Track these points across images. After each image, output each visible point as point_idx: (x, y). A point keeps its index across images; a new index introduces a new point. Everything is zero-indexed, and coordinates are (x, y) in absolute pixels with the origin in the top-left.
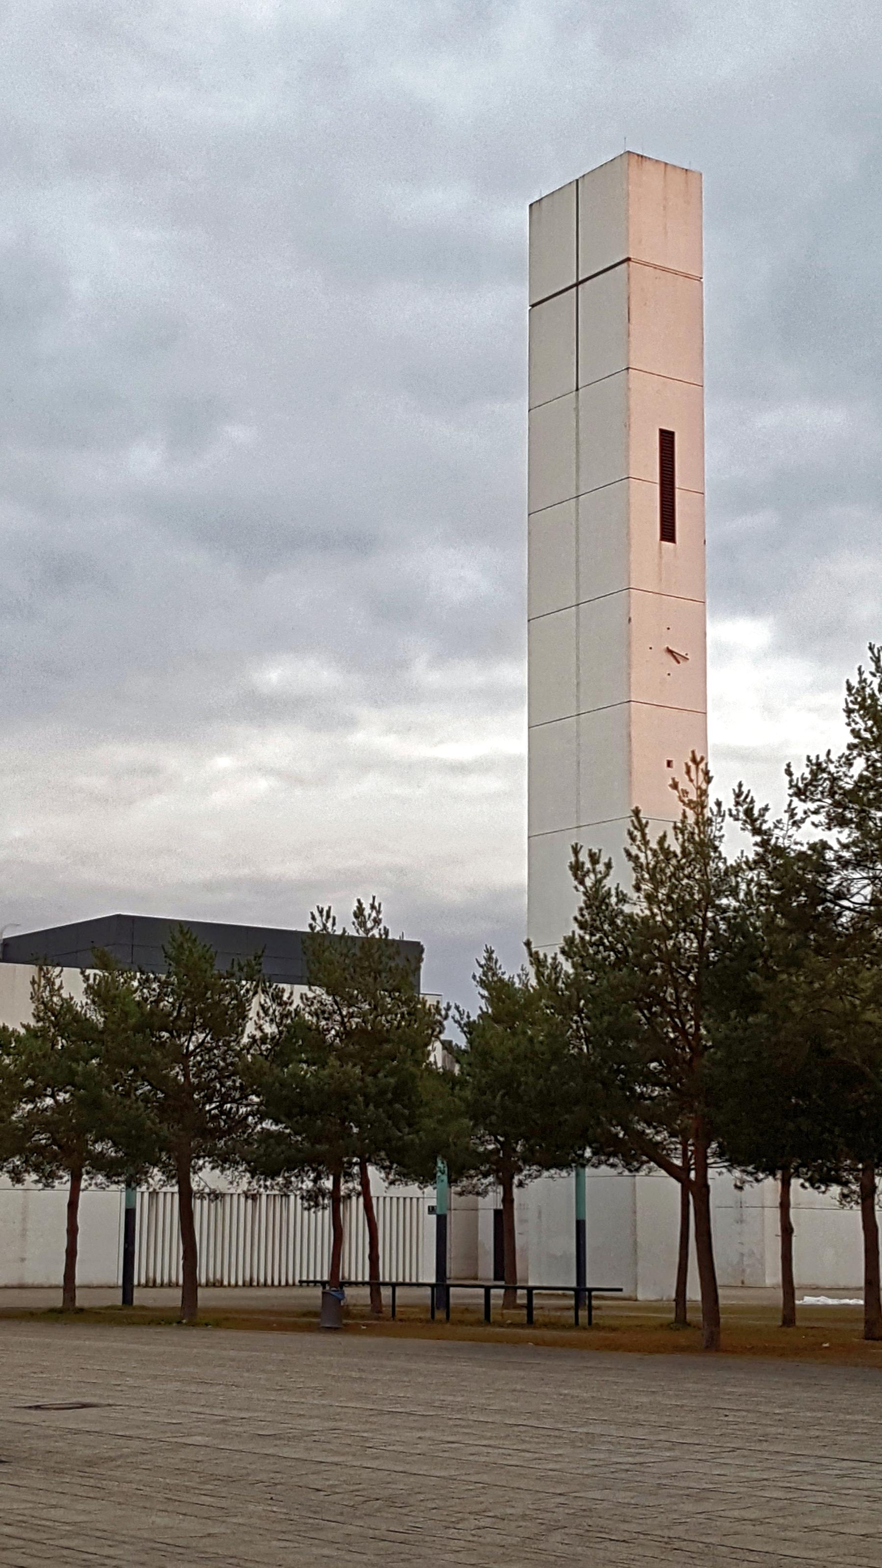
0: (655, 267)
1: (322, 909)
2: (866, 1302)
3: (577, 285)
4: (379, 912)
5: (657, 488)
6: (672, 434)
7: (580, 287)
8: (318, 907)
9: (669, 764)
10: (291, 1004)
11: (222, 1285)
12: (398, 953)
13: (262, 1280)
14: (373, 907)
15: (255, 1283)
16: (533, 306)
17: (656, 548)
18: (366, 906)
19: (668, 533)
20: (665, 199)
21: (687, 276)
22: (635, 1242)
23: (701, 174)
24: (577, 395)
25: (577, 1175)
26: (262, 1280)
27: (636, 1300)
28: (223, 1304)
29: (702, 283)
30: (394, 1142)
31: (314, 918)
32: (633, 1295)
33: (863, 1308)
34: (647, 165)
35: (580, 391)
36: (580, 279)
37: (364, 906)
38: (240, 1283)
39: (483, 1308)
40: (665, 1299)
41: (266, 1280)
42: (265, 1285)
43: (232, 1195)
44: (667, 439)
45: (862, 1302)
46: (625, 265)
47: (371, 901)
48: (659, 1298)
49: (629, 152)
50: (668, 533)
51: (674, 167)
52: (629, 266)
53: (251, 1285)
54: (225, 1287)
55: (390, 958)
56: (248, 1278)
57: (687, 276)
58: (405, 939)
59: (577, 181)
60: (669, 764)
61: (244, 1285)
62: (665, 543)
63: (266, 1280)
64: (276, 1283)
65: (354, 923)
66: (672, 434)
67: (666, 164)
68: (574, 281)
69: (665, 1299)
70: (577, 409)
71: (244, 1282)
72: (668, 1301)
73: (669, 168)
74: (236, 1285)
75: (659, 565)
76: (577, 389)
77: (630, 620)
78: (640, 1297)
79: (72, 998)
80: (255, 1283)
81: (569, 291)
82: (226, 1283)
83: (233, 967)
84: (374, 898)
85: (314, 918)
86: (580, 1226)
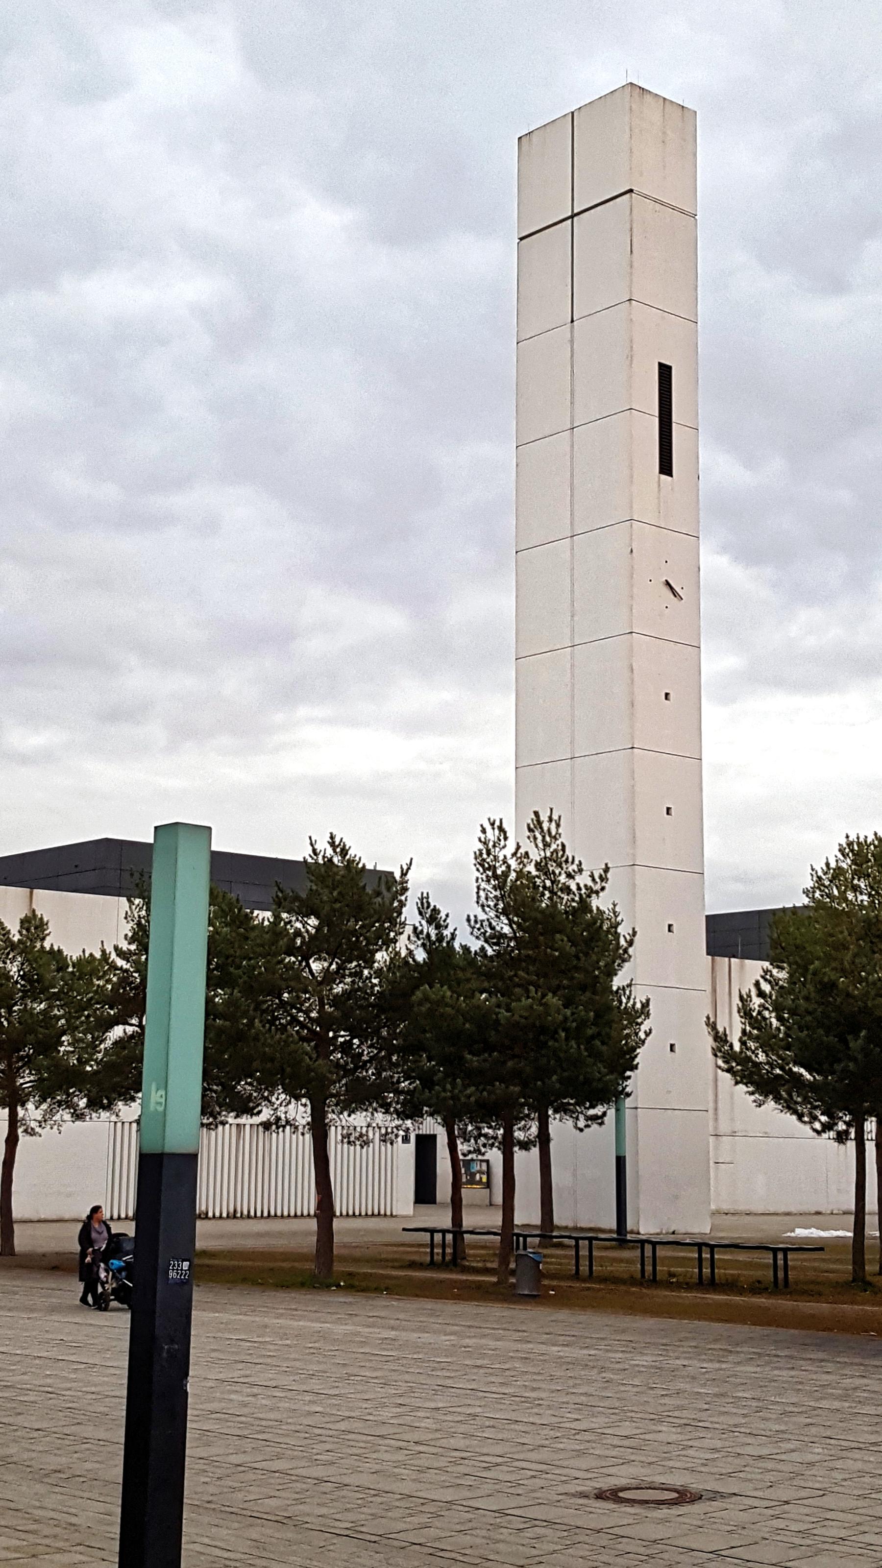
0: (656, 201)
1: (494, 821)
2: (855, 1234)
3: (572, 217)
4: (558, 825)
5: (657, 420)
6: (670, 368)
7: (575, 219)
8: (489, 819)
9: (667, 695)
10: (446, 927)
11: (207, 1217)
12: (580, 871)
13: (245, 1212)
14: (550, 820)
15: (239, 1215)
16: (521, 239)
17: (657, 479)
18: (544, 817)
19: (666, 468)
20: (664, 133)
21: (682, 212)
22: (164, 1136)
23: (696, 112)
24: (572, 328)
25: (617, 1110)
26: (245, 1212)
27: (638, 1233)
28: (250, 1244)
29: (696, 220)
30: (595, 1084)
31: (484, 831)
32: (635, 1229)
33: (851, 1241)
34: (648, 98)
35: (575, 323)
36: (575, 211)
37: (542, 819)
38: (225, 1215)
39: (639, 1259)
40: (664, 1232)
41: (249, 1212)
42: (249, 1216)
43: (244, 1125)
44: (665, 372)
45: (851, 1234)
46: (628, 196)
47: (548, 814)
48: (658, 1231)
49: (631, 84)
50: (666, 468)
51: (671, 102)
52: (631, 196)
53: (235, 1217)
54: (210, 1219)
55: (570, 876)
56: (232, 1210)
57: (682, 212)
58: (378, 868)
59: (573, 113)
60: (667, 695)
61: (228, 1216)
62: (663, 477)
63: (249, 1212)
64: (266, 1214)
65: (529, 838)
66: (670, 368)
67: (665, 99)
68: (570, 214)
69: (664, 1232)
70: (572, 341)
71: (228, 1214)
72: (667, 1233)
73: (667, 102)
74: (221, 1217)
75: (659, 498)
76: (572, 321)
77: (632, 551)
78: (642, 1232)
79: (47, 924)
80: (239, 1215)
81: (564, 223)
82: (210, 1214)
83: (379, 886)
84: (551, 810)
85: (484, 831)
86: (620, 1162)
